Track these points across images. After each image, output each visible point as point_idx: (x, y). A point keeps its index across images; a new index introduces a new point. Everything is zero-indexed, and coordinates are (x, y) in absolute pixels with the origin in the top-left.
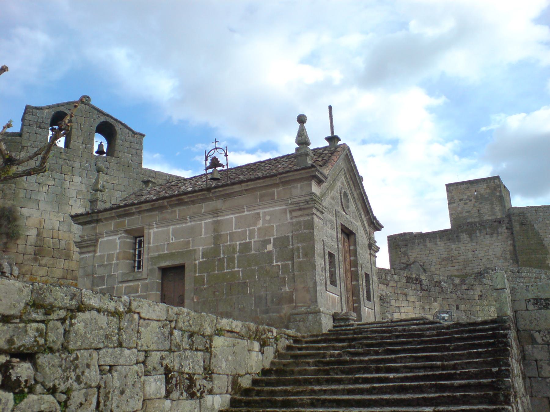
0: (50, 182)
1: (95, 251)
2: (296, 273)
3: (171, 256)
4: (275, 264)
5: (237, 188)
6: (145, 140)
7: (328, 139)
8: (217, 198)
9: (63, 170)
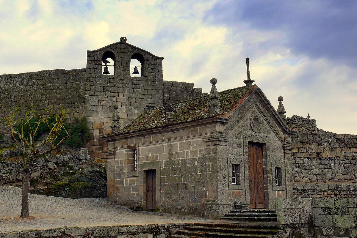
0: (105, 98)
1: (114, 158)
2: (208, 180)
3: (149, 164)
4: (198, 173)
5: (178, 127)
6: (163, 61)
7: (245, 82)
8: (170, 131)
9: (112, 90)
